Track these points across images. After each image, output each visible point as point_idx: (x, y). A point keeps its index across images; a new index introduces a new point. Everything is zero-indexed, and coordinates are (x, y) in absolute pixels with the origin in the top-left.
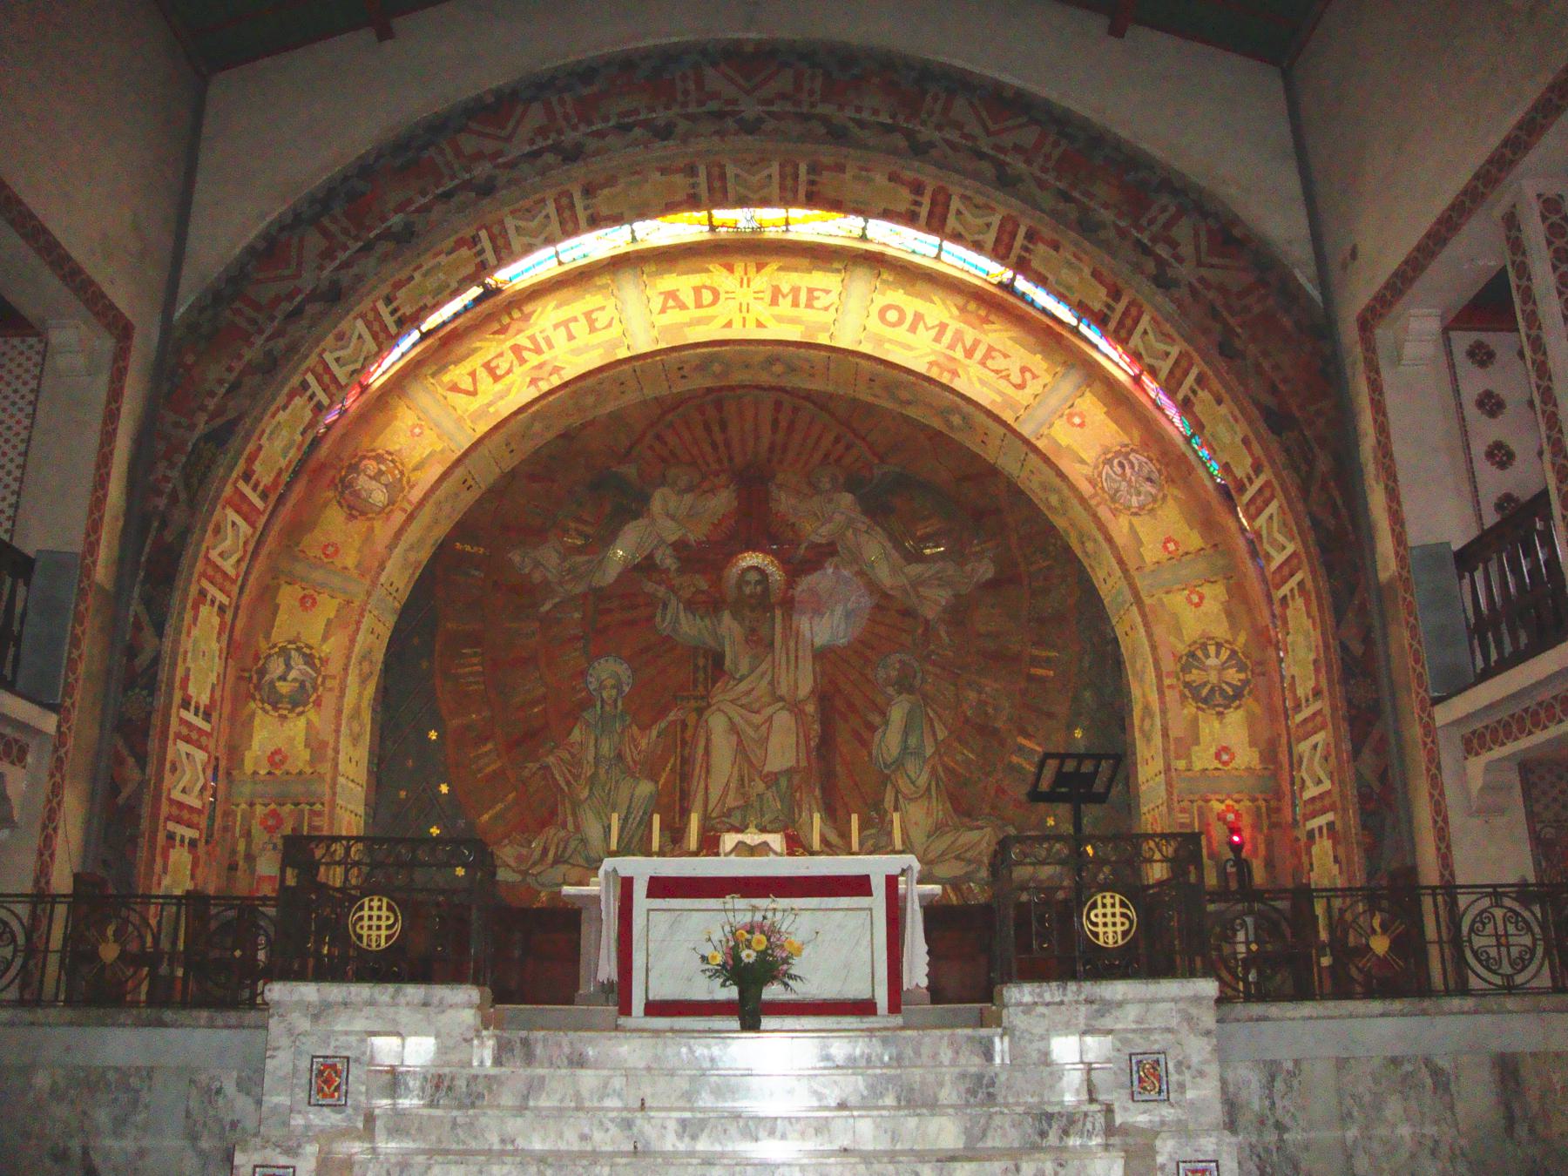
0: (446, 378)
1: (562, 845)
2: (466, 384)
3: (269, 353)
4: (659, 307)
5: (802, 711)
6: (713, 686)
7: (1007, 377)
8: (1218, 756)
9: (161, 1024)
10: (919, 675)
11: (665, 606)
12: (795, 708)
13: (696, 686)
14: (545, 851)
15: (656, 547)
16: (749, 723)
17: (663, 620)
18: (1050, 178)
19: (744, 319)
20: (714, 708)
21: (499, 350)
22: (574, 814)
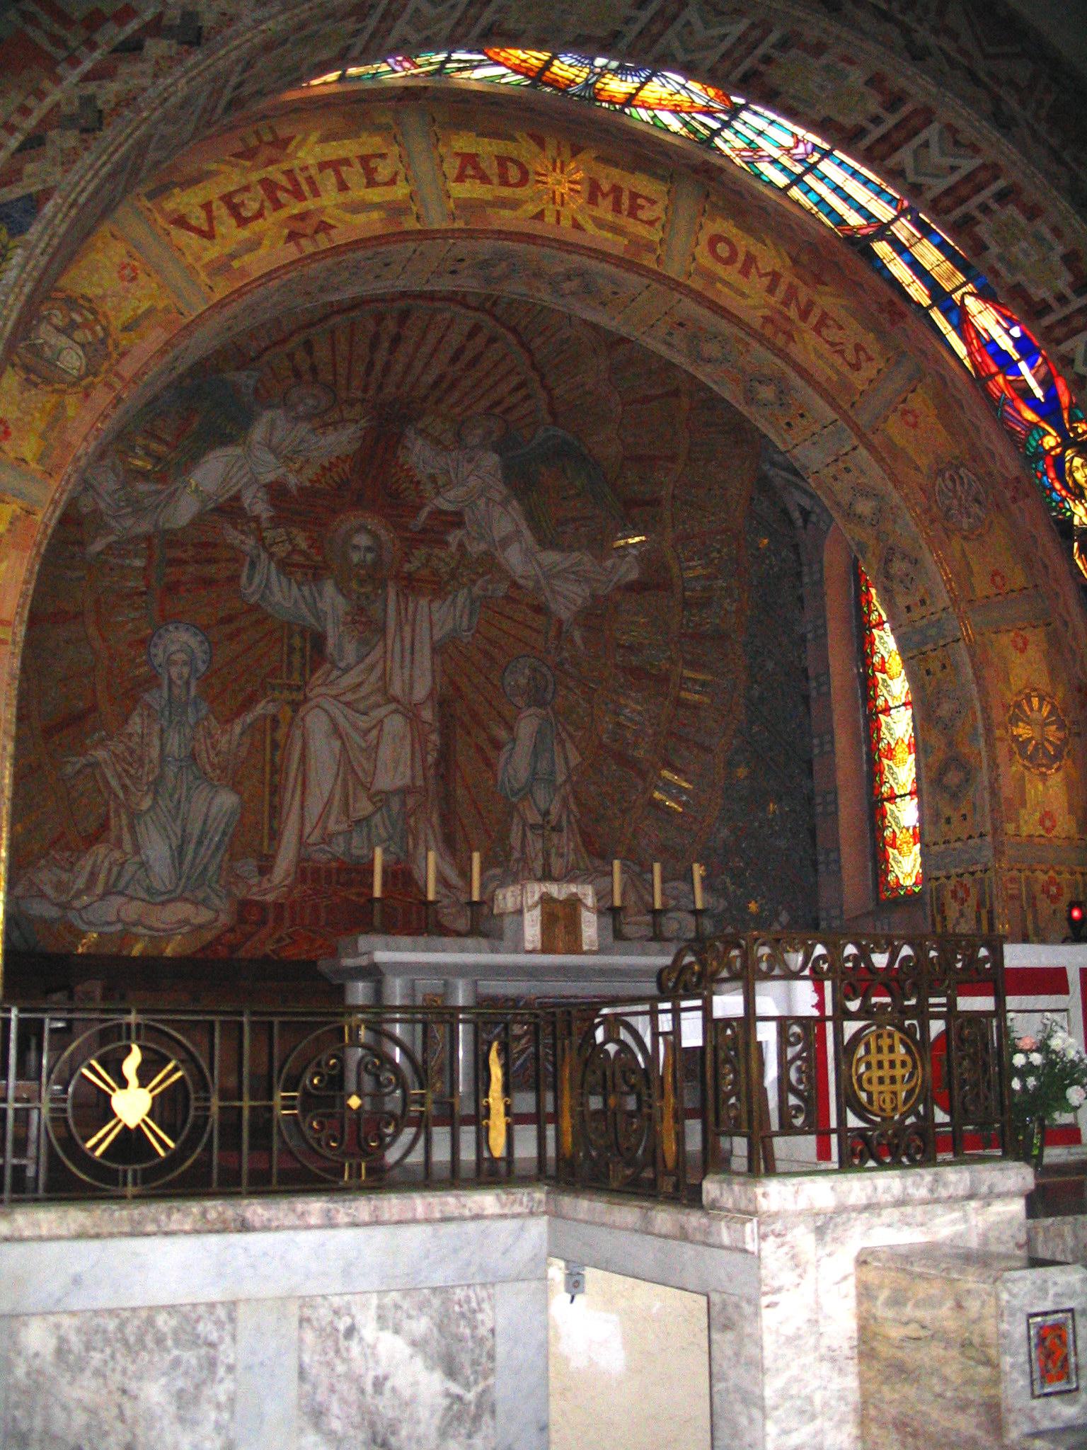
0: (169, 206)
1: (115, 870)
2: (198, 218)
3: (88, 101)
4: (455, 172)
5: (418, 716)
6: (313, 672)
7: (841, 352)
8: (1042, 822)
9: (245, 1227)
10: (551, 687)
11: (253, 565)
12: (411, 714)
13: (290, 672)
14: (93, 876)
15: (246, 486)
16: (354, 726)
17: (250, 579)
18: (1042, 128)
19: (558, 213)
20: (312, 703)
21: (244, 182)
22: (132, 828)
